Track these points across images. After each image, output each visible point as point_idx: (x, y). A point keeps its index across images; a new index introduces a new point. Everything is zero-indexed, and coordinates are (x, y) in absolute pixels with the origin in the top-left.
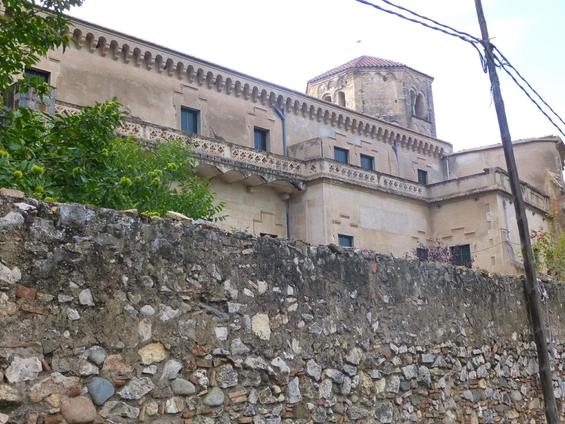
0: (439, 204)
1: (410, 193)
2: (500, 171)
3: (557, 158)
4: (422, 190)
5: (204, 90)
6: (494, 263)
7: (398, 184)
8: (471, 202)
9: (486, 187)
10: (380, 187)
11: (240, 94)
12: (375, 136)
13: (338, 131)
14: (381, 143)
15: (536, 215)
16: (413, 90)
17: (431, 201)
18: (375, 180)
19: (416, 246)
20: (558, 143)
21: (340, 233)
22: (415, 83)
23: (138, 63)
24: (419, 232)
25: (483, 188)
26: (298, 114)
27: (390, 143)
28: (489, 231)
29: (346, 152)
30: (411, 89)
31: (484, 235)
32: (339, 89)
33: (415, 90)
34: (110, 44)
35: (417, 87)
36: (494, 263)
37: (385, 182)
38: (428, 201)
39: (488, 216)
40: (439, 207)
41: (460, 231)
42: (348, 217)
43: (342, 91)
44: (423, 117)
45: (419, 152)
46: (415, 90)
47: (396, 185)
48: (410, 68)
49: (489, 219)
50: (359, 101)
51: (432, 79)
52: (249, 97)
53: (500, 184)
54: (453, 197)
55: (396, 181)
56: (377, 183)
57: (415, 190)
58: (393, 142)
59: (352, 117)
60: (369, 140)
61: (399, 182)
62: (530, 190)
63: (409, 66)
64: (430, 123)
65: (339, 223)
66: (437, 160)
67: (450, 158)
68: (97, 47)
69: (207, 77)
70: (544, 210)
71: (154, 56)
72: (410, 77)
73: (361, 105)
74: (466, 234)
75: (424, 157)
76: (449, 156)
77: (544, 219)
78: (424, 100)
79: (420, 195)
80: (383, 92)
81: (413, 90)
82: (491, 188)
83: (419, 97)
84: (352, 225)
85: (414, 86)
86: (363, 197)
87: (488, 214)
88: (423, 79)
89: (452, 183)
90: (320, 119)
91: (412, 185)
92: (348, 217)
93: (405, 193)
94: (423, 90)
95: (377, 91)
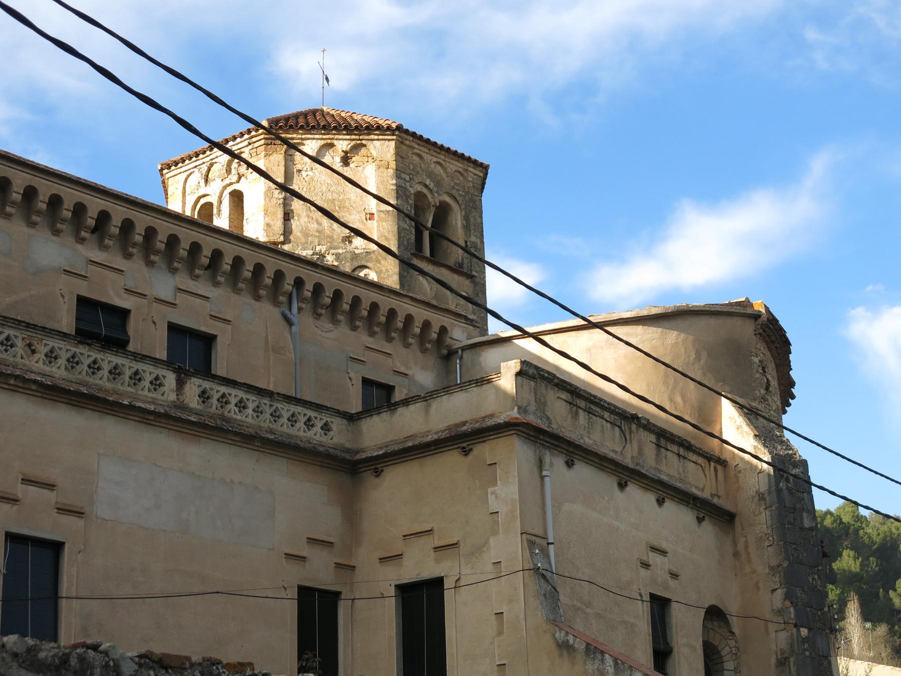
0: (377, 464)
1: (293, 431)
2: (531, 371)
3: (756, 360)
4: (334, 427)
5: (135, 270)
6: (500, 633)
7: (251, 406)
8: (452, 459)
9: (491, 416)
10: (184, 408)
11: (340, 317)
12: (221, 279)
13: (99, 256)
14: (246, 299)
15: (668, 504)
16: (425, 190)
17: (358, 457)
18: (165, 389)
19: (297, 576)
20: (760, 321)
21: (15, 530)
22: (431, 175)
23: (197, 271)
24: (312, 541)
25: (484, 418)
26: (393, 339)
27: (276, 303)
28: (492, 541)
29: (208, 340)
30: (419, 188)
31: (479, 549)
32: (231, 184)
33: (431, 190)
34: (95, 217)
35: (438, 184)
36: (500, 633)
37: (204, 396)
38: (348, 456)
39: (491, 498)
40: (378, 473)
41: (423, 540)
42: (51, 486)
43: (236, 187)
44: (451, 263)
45: (372, 334)
46: (431, 190)
47: (241, 405)
48: (414, 135)
49: (494, 505)
50: (274, 214)
51: (484, 168)
52: (134, 251)
53: (532, 408)
54: (410, 444)
55: (242, 394)
56: (173, 397)
57: (51, 356)
58: (283, 299)
59: (386, 303)
60: (203, 287)
61: (252, 401)
62: (653, 438)
63: (411, 129)
64: (470, 277)
65: (14, 501)
66: (431, 360)
67: (467, 355)
68: (94, 231)
69: (232, 266)
70: (706, 495)
71: (185, 245)
72: (415, 158)
73: (278, 224)
74: (437, 549)
75: (387, 348)
76: (464, 349)
77: (700, 520)
78: (457, 219)
79: (324, 439)
80: (339, 193)
81: (425, 190)
82: (501, 420)
83: (443, 211)
84: (63, 510)
85: (428, 182)
86: (112, 430)
87: (493, 493)
88: (454, 166)
89: (412, 407)
90: (358, 323)
91: (299, 409)
92: (51, 486)
93: (271, 431)
94: (454, 192)
95: (324, 188)
